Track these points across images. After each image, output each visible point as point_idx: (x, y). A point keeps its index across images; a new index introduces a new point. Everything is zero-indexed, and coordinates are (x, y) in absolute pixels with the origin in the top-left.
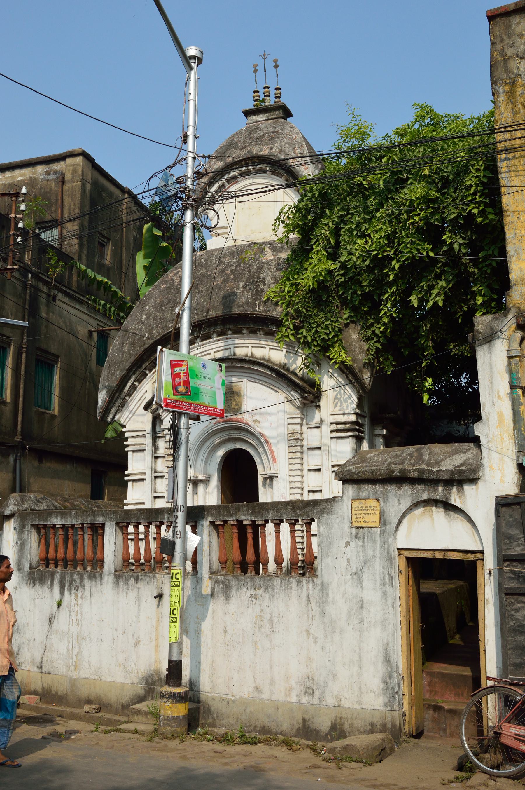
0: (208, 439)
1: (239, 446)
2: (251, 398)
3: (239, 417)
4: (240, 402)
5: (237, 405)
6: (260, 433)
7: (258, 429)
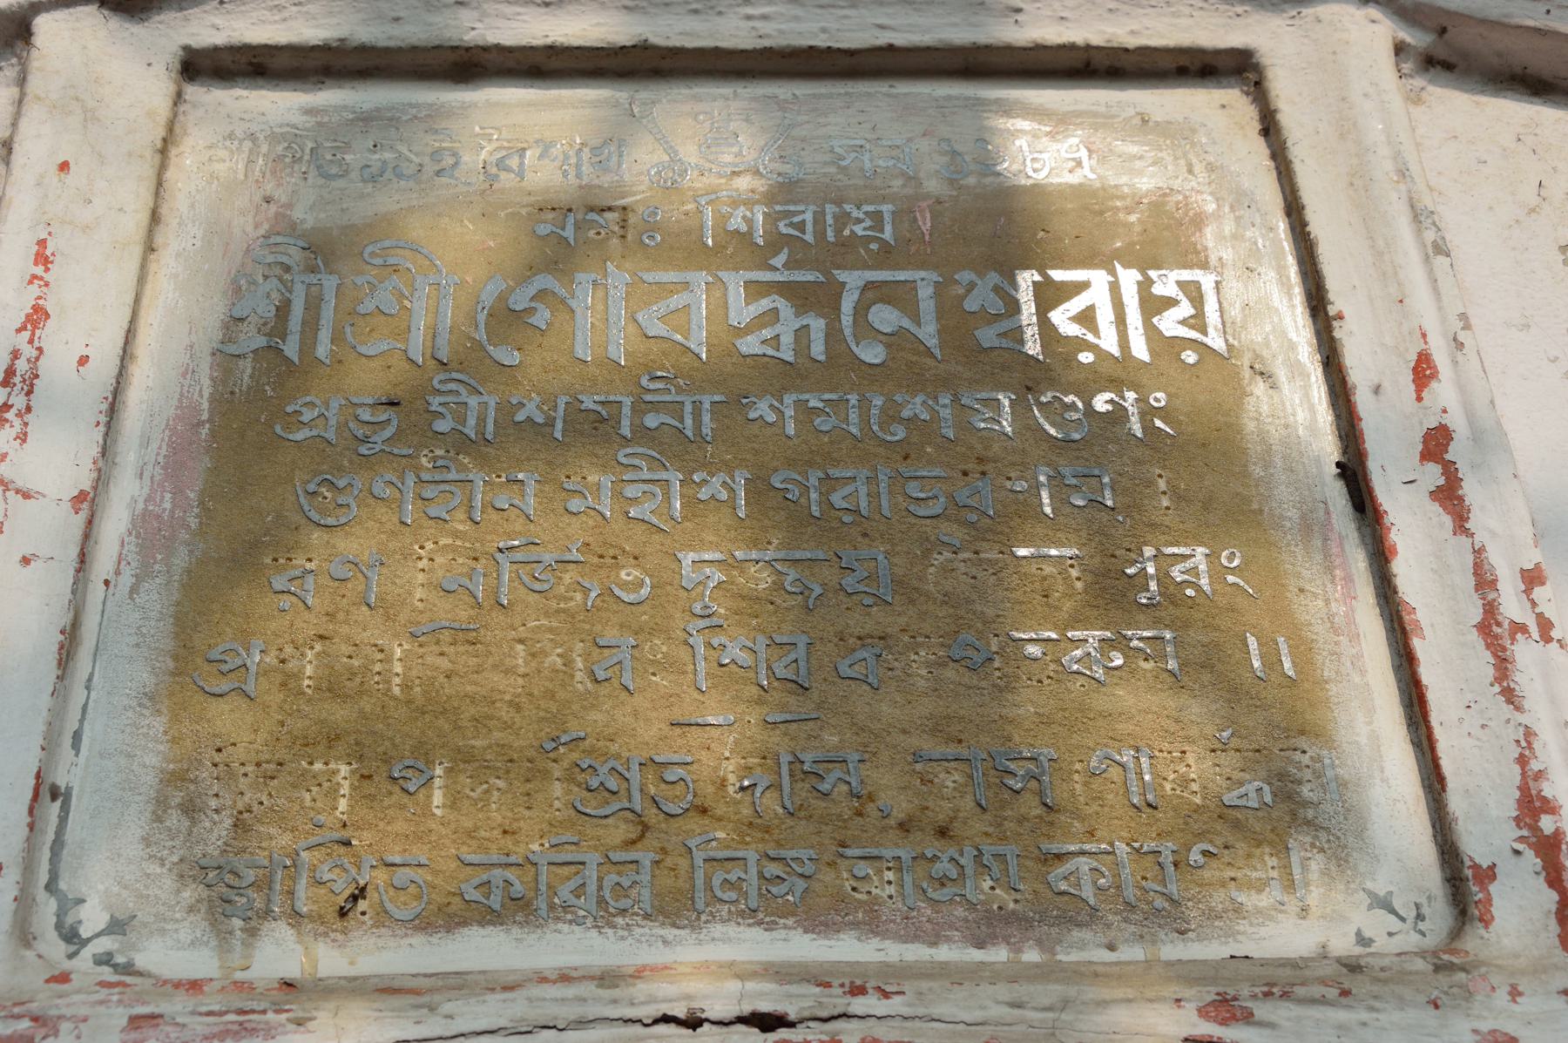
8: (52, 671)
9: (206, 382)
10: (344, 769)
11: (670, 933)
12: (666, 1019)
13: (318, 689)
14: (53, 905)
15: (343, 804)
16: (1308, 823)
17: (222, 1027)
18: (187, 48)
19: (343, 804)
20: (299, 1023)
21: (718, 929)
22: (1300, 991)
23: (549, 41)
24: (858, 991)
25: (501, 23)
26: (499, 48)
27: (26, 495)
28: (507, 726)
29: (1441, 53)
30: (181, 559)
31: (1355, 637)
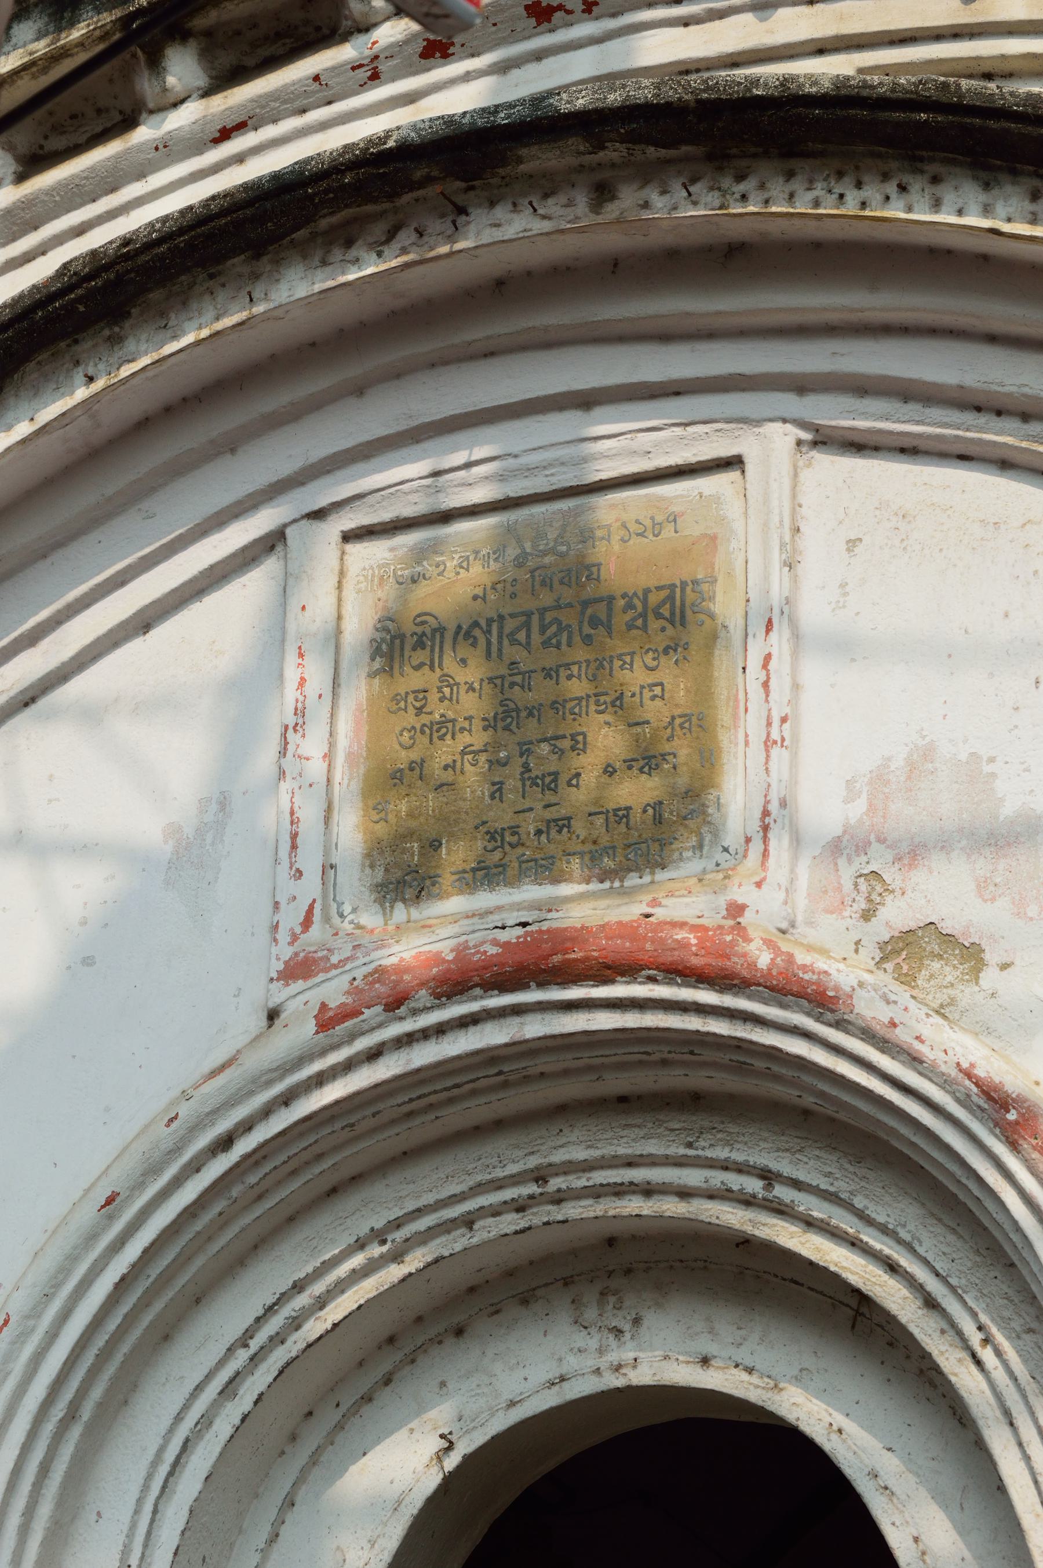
0: (165, 1335)
1: (673, 1354)
2: (844, 648)
3: (678, 904)
4: (699, 724)
5: (647, 759)
6: (995, 1103)
7: (955, 1046)
8: (321, 826)
9: (364, 692)
10: (416, 845)
11: (511, 890)
12: (497, 927)
13: (407, 815)
14: (335, 906)
15: (416, 858)
16: (709, 822)
17: (348, 967)
18: (342, 532)
19: (416, 858)
20: (397, 942)
21: (525, 887)
22: (677, 893)
23: (472, 503)
24: (550, 911)
25: (454, 497)
26: (455, 508)
27: (308, 759)
28: (464, 821)
29: (819, 439)
30: (362, 770)
31: (736, 744)
